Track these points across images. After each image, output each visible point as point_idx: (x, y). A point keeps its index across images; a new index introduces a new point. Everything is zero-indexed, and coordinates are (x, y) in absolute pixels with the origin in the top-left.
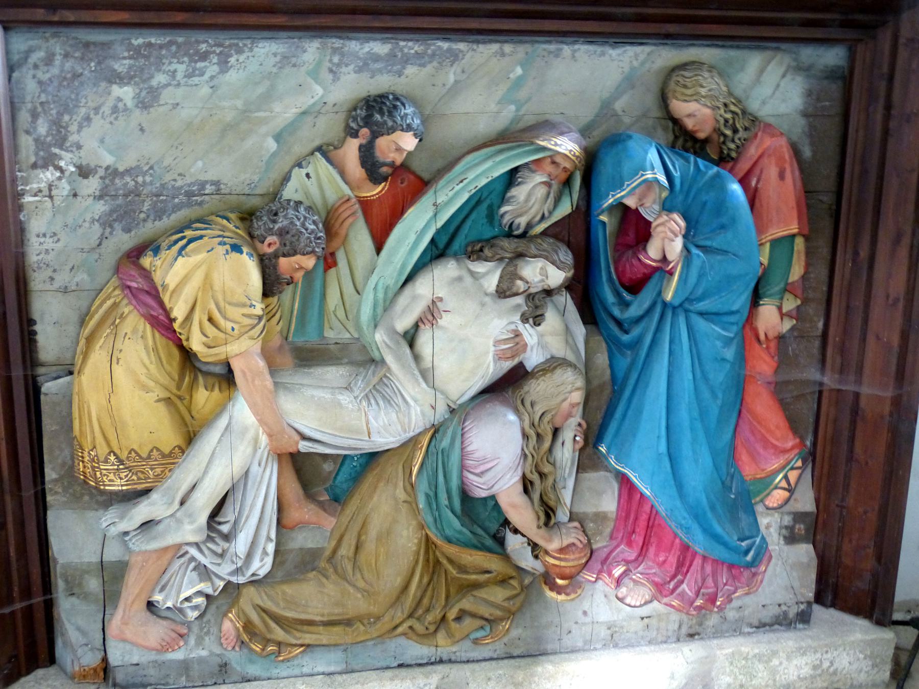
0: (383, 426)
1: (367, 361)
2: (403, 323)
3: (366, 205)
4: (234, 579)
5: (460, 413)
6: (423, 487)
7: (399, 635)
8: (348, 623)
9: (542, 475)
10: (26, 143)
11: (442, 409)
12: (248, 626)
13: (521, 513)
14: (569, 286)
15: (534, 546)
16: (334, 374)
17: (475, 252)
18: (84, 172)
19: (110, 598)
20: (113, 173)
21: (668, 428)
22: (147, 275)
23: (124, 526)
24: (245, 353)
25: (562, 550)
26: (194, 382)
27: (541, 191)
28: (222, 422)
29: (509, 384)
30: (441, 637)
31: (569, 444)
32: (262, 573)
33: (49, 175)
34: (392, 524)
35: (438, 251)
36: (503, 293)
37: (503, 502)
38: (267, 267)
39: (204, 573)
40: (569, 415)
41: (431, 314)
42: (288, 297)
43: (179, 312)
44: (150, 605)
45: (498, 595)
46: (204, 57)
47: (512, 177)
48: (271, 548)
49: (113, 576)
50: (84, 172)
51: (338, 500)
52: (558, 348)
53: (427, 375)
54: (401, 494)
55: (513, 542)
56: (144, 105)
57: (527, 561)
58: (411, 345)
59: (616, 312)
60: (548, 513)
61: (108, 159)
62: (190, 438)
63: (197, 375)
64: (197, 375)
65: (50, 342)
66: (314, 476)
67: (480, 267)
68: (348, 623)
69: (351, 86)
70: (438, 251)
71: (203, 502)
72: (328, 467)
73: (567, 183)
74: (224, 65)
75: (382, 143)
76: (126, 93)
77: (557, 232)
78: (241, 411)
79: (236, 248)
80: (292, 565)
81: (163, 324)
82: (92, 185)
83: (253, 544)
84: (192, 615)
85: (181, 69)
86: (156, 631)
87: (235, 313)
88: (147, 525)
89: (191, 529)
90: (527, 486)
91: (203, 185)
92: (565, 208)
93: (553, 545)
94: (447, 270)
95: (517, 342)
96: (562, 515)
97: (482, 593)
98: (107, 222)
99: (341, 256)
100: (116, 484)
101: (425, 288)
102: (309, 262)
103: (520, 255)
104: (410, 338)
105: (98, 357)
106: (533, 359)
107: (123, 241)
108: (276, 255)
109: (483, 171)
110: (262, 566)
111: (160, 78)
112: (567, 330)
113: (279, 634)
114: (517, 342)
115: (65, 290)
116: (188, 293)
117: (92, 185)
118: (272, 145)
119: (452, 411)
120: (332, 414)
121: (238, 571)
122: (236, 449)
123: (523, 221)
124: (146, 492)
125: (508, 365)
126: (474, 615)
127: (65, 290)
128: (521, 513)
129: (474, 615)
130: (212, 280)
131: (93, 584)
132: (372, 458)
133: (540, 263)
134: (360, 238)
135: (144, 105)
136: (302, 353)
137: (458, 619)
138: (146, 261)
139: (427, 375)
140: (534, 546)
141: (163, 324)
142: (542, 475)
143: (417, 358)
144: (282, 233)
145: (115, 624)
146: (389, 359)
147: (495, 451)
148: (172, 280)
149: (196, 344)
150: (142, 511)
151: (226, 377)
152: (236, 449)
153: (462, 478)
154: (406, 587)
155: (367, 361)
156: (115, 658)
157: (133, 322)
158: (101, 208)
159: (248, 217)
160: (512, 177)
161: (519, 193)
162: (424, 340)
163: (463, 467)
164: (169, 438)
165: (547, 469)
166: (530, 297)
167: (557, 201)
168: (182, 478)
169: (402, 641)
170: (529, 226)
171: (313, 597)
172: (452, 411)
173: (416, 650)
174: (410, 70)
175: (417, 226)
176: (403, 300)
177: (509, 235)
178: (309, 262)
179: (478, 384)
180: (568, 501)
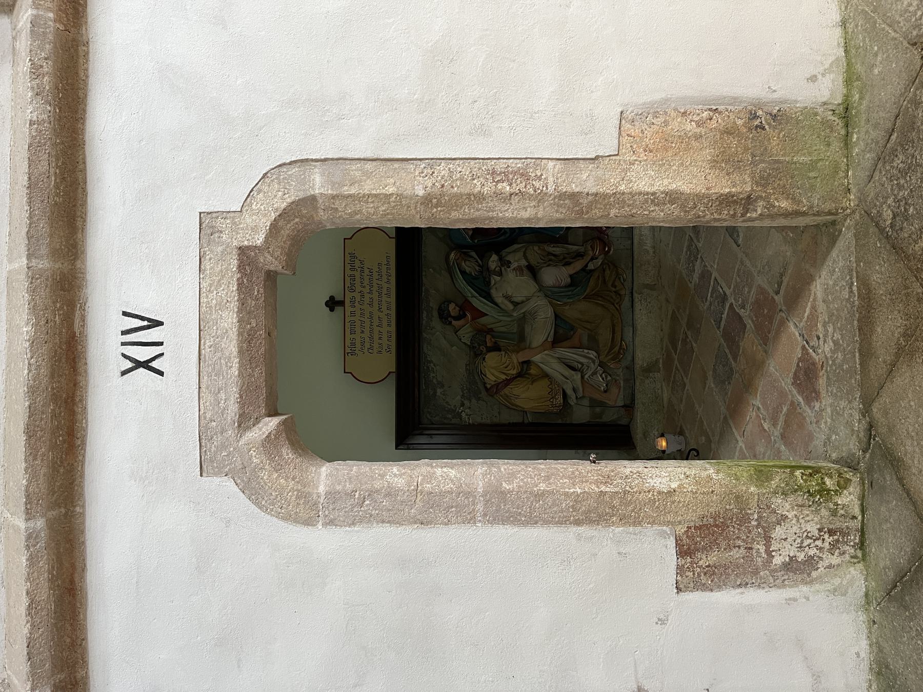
0: (544, 312)
1: (523, 319)
2: (511, 307)
3: (473, 319)
4: (597, 364)
5: (541, 288)
6: (565, 300)
7: (892, 368)
8: (613, 326)
9: (564, 258)
10: (454, 421)
11: (539, 294)
12: (613, 359)
13: (578, 265)
14: (497, 253)
15: (592, 259)
16: (527, 329)
17: (488, 283)
18: (463, 405)
19: (602, 404)
20: (463, 396)
21: (307, 160)
22: (492, 386)
23: (574, 397)
24: (522, 356)
25: (593, 250)
26: (529, 374)
27: (467, 263)
28: (541, 365)
29: (533, 272)
30: (623, 292)
31: (554, 249)
32: (595, 354)
33: (463, 415)
34: (575, 311)
35: (488, 296)
36: (500, 274)
37: (572, 272)
38: (490, 350)
39: (594, 373)
40: (544, 250)
41: (508, 298)
42: (502, 342)
43: (504, 377)
44: (605, 392)
45: (608, 272)
46: (428, 367)
47: (463, 273)
48: (586, 351)
49: (594, 403)
50: (463, 405)
51: (572, 328)
52: (520, 254)
53: (528, 299)
54: (567, 307)
55: (591, 266)
56: (443, 386)
57: (599, 262)
58: (518, 304)
59: (508, 235)
60: (579, 255)
61: (459, 397)
62: (546, 375)
63: (525, 371)
64: (525, 371)
65: (516, 418)
66: (562, 335)
67: (493, 282)
68: (613, 326)
69: (436, 323)
70: (488, 296)
71: (567, 372)
72: (561, 331)
73: (465, 253)
74: (430, 362)
75: (452, 314)
76: (439, 391)
77: (481, 257)
78: (537, 359)
79: (484, 359)
80: (593, 343)
81: (507, 382)
82: (467, 403)
83: (585, 357)
84: (609, 378)
85: (432, 375)
86: (614, 390)
87: (504, 360)
88: (574, 390)
89: (577, 377)
90: (567, 264)
91: (467, 369)
92: (473, 254)
93: (591, 253)
94: (493, 292)
95: (519, 269)
96: (582, 249)
97: (607, 278)
98: (479, 399)
99: (489, 327)
100: (560, 399)
101: (499, 300)
102: (488, 337)
103: (488, 269)
104: (516, 304)
105: (518, 402)
106: (524, 263)
107: (484, 394)
108: (486, 347)
109: (461, 283)
110: (592, 354)
111: (435, 381)
112: (514, 251)
113: (617, 348)
114: (519, 269)
115: (499, 413)
116: (497, 374)
117: (467, 403)
118: (454, 348)
119: (540, 290)
120: (541, 331)
121: (594, 362)
122: (548, 362)
123: (477, 268)
124: (563, 390)
125: (525, 271)
126: (614, 281)
127: (499, 413)
128: (578, 265)
129: (614, 281)
130: (494, 367)
131: (598, 410)
132: (556, 316)
133: (490, 263)
134: (483, 320)
135: (443, 386)
136: (521, 340)
137: (615, 287)
138: (489, 386)
139: (528, 299)
140: (592, 259)
141: (507, 382)
142: (564, 258)
143: (523, 302)
144: (479, 345)
145: (611, 403)
146: (522, 311)
147: (553, 276)
148: (493, 379)
149: (515, 372)
150: (569, 392)
151: (528, 363)
152: (548, 362)
153: (566, 287)
154: (602, 306)
155: (523, 319)
156: (622, 404)
157: (506, 391)
158: (474, 401)
159: (476, 355)
160: (463, 273)
161: (468, 270)
162: (516, 300)
163: (559, 287)
164: (545, 382)
165: (562, 257)
166: (502, 265)
167: (472, 257)
168: (559, 378)
169: (622, 306)
170: (479, 266)
171: (604, 336)
172: (540, 290)
173: (626, 302)
174: (431, 305)
175: (478, 303)
176: (503, 307)
177: (482, 272)
178: (488, 337)
179: (532, 282)
180: (577, 247)
